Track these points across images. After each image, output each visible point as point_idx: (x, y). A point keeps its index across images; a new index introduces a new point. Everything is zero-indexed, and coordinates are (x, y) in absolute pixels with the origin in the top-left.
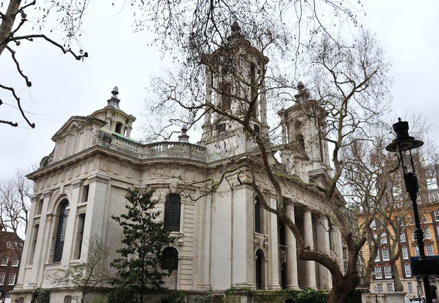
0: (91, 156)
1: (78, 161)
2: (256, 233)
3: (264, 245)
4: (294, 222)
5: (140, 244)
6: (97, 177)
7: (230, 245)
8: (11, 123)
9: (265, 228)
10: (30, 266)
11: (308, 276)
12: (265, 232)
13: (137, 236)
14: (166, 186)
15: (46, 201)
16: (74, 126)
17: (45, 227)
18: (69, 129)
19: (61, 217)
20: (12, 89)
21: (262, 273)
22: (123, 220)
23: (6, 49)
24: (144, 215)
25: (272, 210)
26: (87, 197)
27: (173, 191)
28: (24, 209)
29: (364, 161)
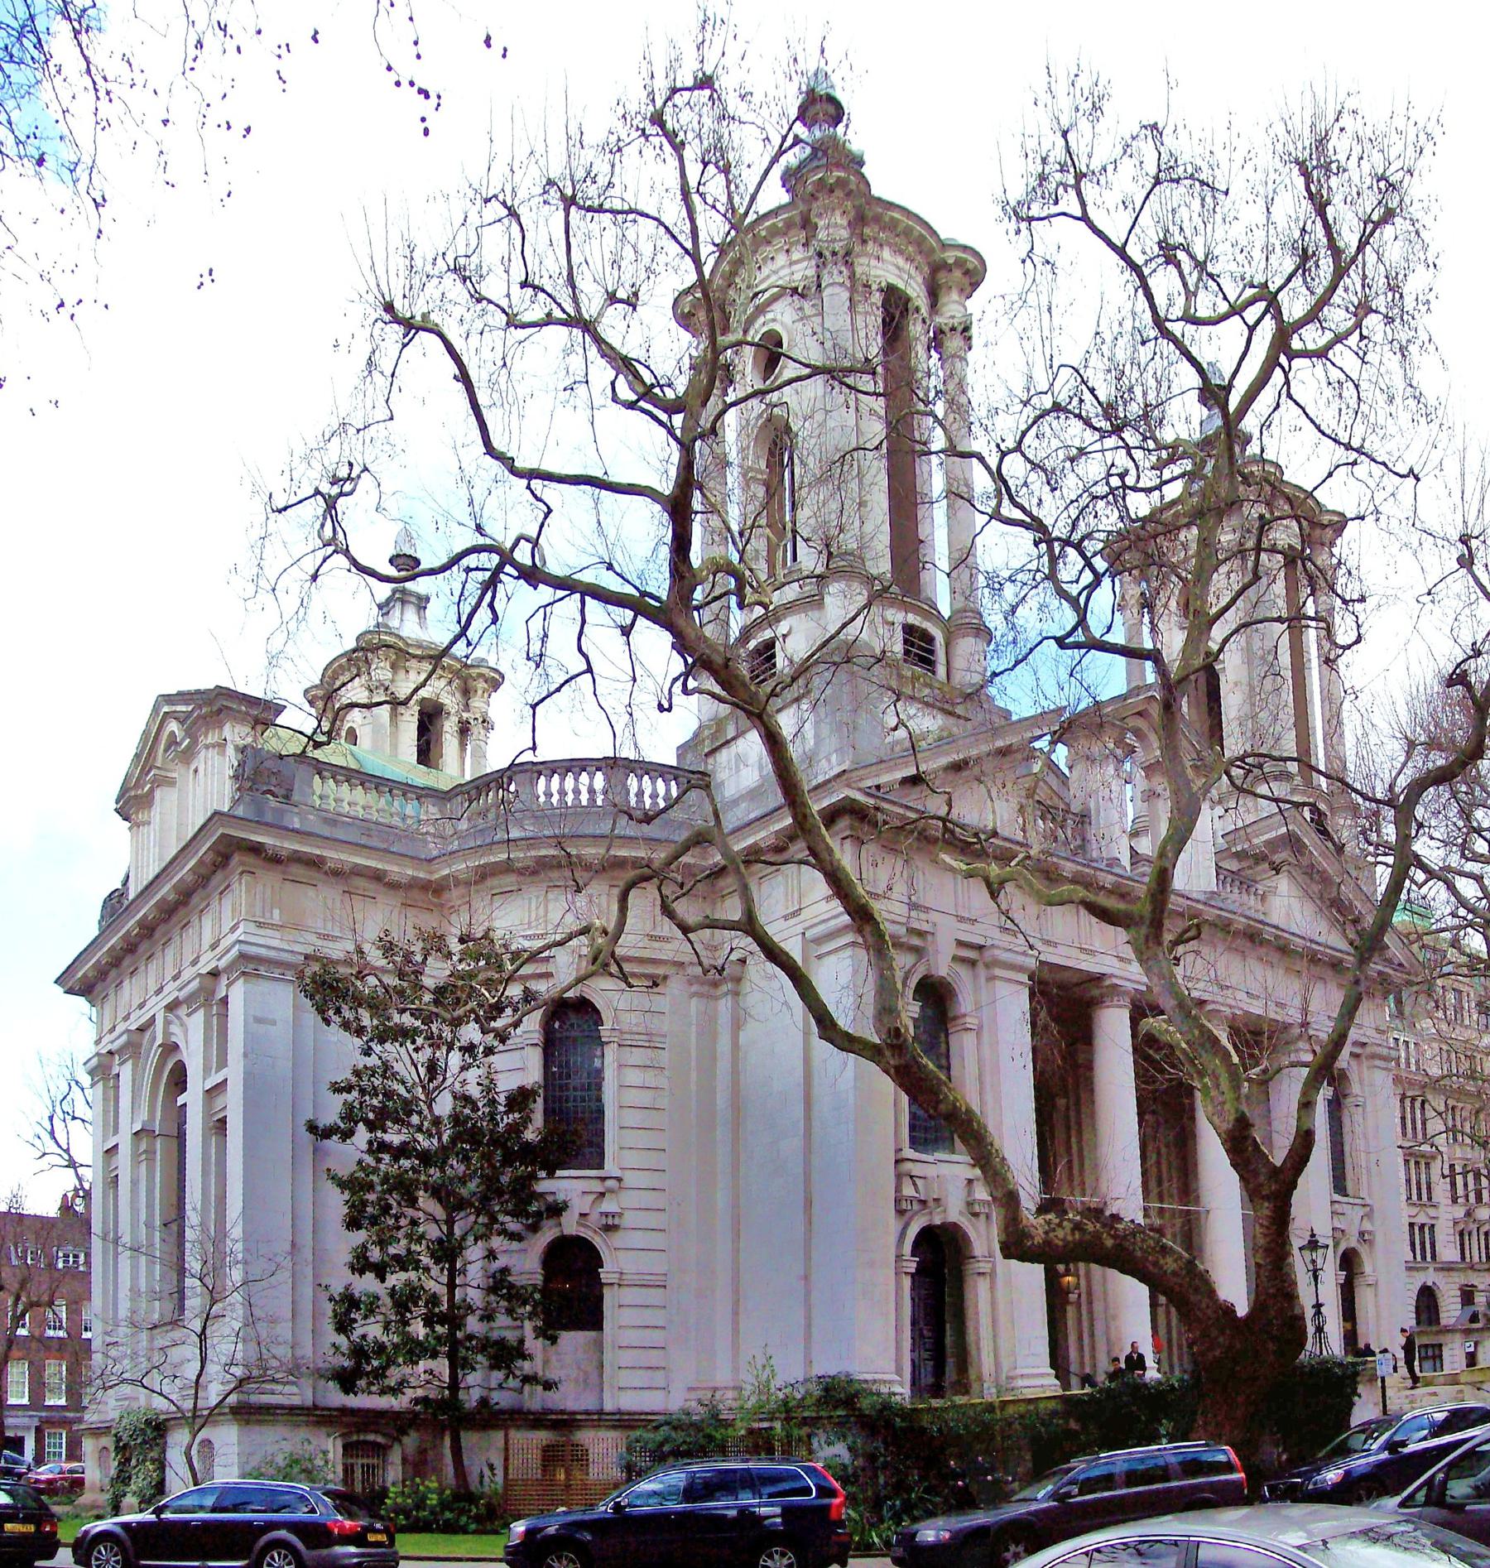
2: (908, 1153)
6: (243, 956)
15: (126, 1072)
16: (173, 741)
17: (135, 1183)
21: (970, 1325)
29: (803, 514)
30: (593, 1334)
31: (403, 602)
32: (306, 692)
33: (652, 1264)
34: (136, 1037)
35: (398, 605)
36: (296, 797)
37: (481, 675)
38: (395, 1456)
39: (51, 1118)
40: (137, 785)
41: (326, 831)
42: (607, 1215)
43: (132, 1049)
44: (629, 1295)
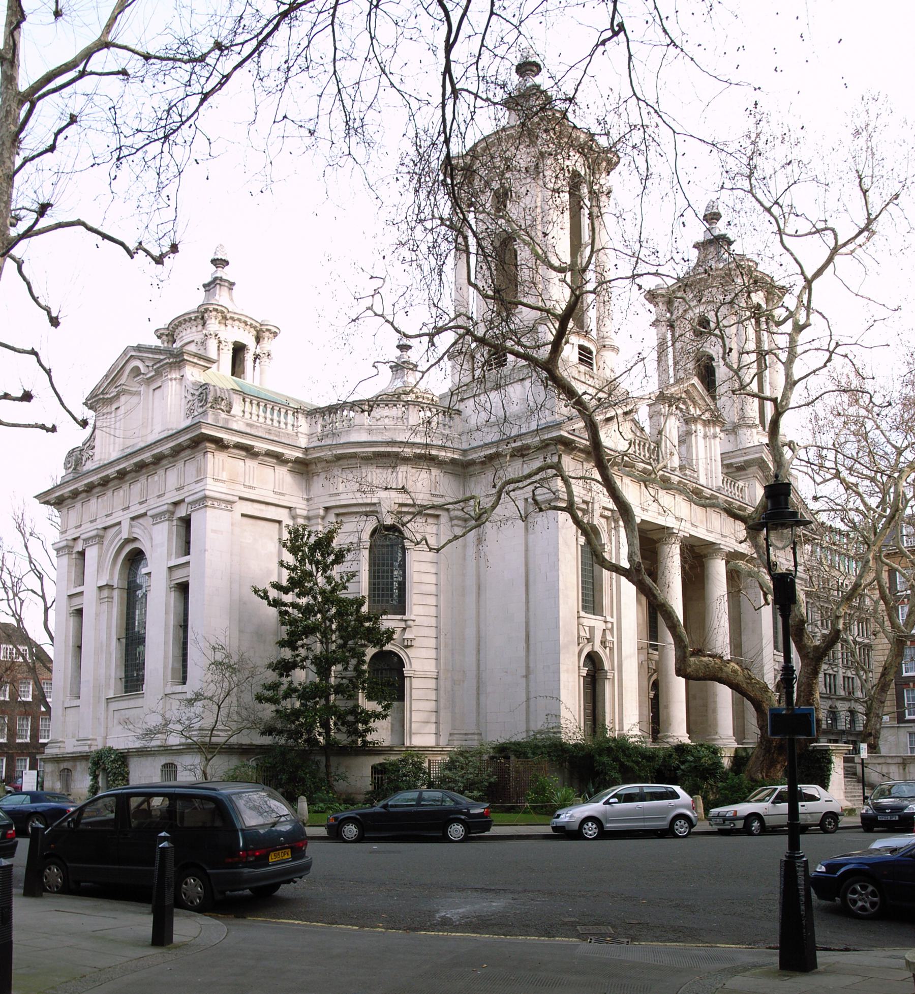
0: (188, 447)
1: (158, 460)
2: (582, 614)
3: (603, 643)
4: (659, 615)
5: (318, 648)
7: (523, 644)
8: (43, 427)
9: (606, 601)
10: (76, 702)
11: (715, 711)
12: (606, 611)
13: (310, 631)
14: (371, 510)
15: (92, 554)
16: (136, 371)
18: (123, 380)
19: (133, 596)
20: (33, 352)
22: (273, 594)
23: (8, 259)
24: (321, 580)
25: (616, 569)
26: (188, 543)
27: (389, 521)
28: (34, 570)
32: (157, 330)
37: (267, 330)
41: (248, 430)
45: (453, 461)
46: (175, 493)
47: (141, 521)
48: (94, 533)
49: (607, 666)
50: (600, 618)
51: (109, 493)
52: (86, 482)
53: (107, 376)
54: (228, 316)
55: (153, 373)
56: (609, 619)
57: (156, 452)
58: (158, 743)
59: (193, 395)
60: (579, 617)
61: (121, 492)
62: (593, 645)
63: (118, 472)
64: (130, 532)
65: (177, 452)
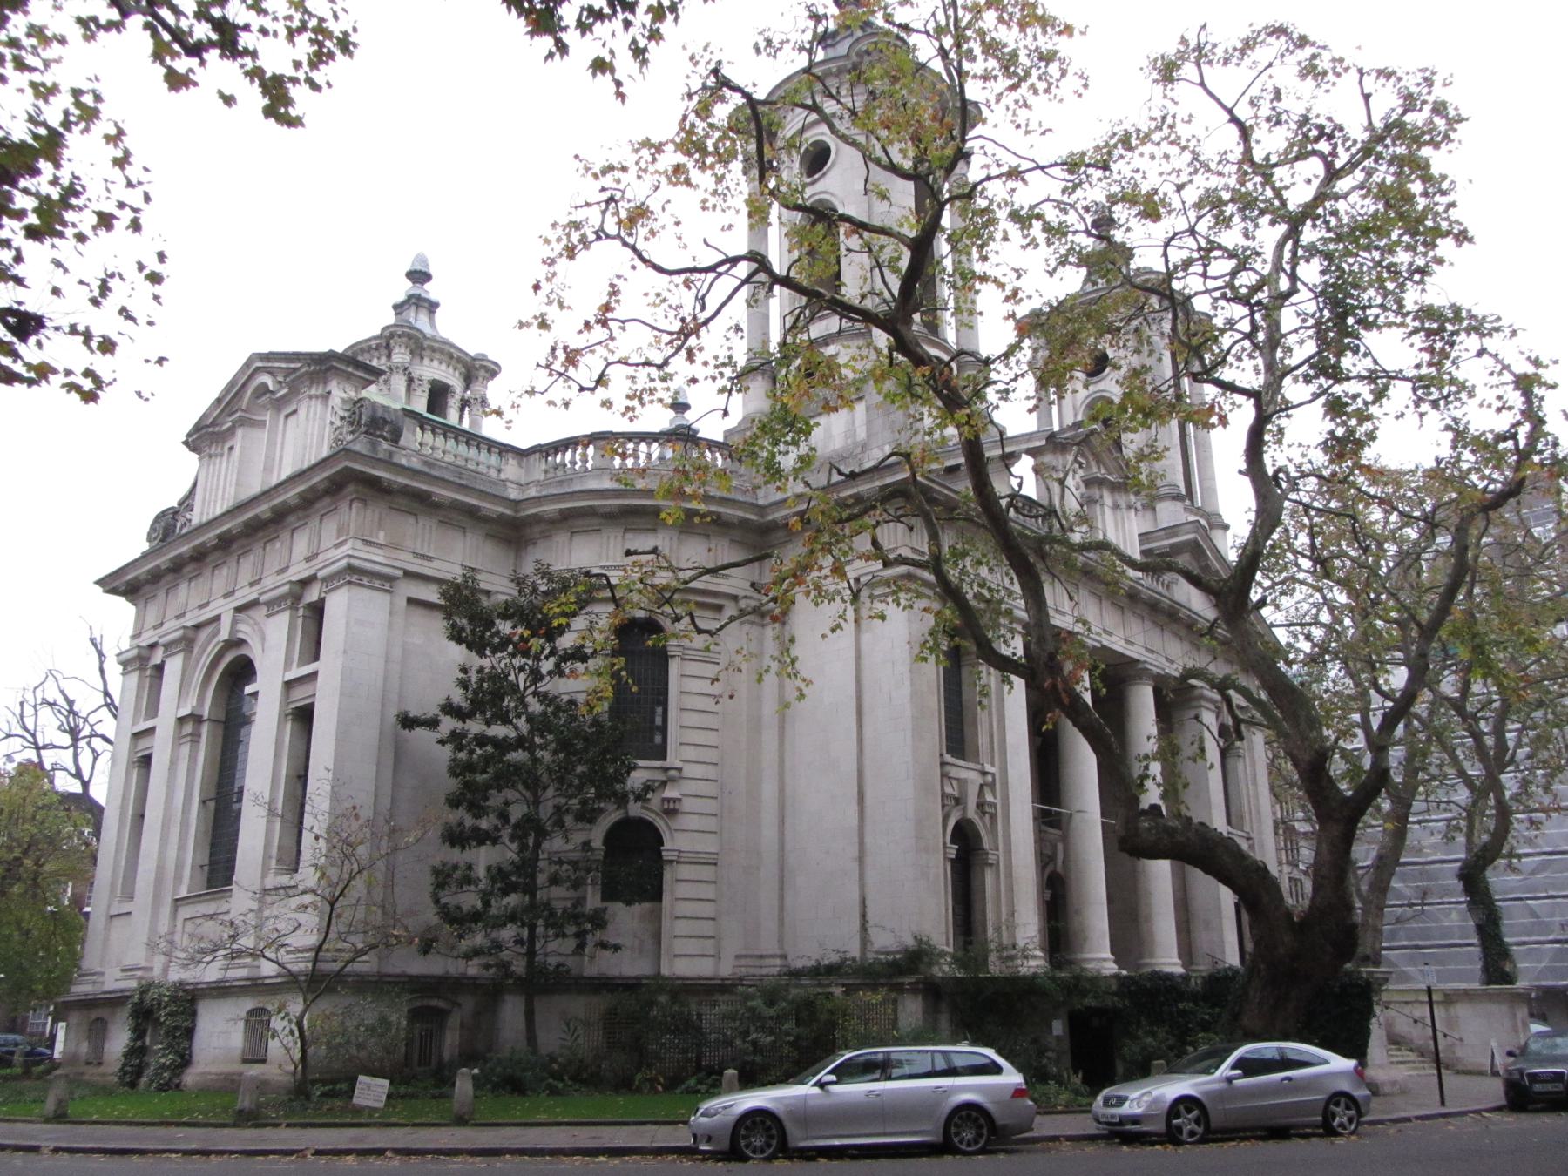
2: (948, 758)
3: (981, 805)
9: (983, 740)
11: (1148, 919)
15: (174, 666)
16: (263, 390)
17: (173, 763)
30: (647, 906)
31: (418, 306)
33: (707, 845)
34: (191, 634)
35: (413, 308)
36: (402, 442)
38: (454, 1021)
39: (22, 704)
40: (213, 424)
41: (426, 470)
42: (669, 800)
43: (187, 642)
44: (685, 871)
45: (744, 523)
46: (304, 565)
47: (252, 613)
48: (179, 634)
49: (986, 843)
50: (971, 765)
51: (207, 573)
52: (172, 555)
53: (219, 400)
54: (426, 344)
55: (285, 391)
56: (988, 768)
57: (275, 502)
58: (243, 973)
59: (342, 418)
60: (943, 764)
61: (225, 571)
62: (965, 810)
63: (219, 537)
64: (233, 630)
65: (308, 503)
